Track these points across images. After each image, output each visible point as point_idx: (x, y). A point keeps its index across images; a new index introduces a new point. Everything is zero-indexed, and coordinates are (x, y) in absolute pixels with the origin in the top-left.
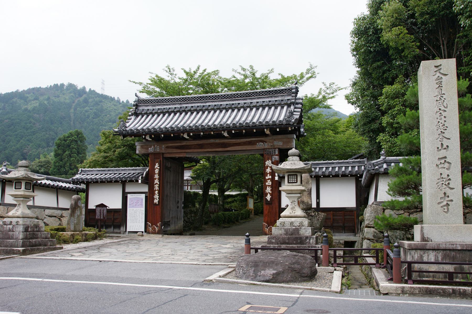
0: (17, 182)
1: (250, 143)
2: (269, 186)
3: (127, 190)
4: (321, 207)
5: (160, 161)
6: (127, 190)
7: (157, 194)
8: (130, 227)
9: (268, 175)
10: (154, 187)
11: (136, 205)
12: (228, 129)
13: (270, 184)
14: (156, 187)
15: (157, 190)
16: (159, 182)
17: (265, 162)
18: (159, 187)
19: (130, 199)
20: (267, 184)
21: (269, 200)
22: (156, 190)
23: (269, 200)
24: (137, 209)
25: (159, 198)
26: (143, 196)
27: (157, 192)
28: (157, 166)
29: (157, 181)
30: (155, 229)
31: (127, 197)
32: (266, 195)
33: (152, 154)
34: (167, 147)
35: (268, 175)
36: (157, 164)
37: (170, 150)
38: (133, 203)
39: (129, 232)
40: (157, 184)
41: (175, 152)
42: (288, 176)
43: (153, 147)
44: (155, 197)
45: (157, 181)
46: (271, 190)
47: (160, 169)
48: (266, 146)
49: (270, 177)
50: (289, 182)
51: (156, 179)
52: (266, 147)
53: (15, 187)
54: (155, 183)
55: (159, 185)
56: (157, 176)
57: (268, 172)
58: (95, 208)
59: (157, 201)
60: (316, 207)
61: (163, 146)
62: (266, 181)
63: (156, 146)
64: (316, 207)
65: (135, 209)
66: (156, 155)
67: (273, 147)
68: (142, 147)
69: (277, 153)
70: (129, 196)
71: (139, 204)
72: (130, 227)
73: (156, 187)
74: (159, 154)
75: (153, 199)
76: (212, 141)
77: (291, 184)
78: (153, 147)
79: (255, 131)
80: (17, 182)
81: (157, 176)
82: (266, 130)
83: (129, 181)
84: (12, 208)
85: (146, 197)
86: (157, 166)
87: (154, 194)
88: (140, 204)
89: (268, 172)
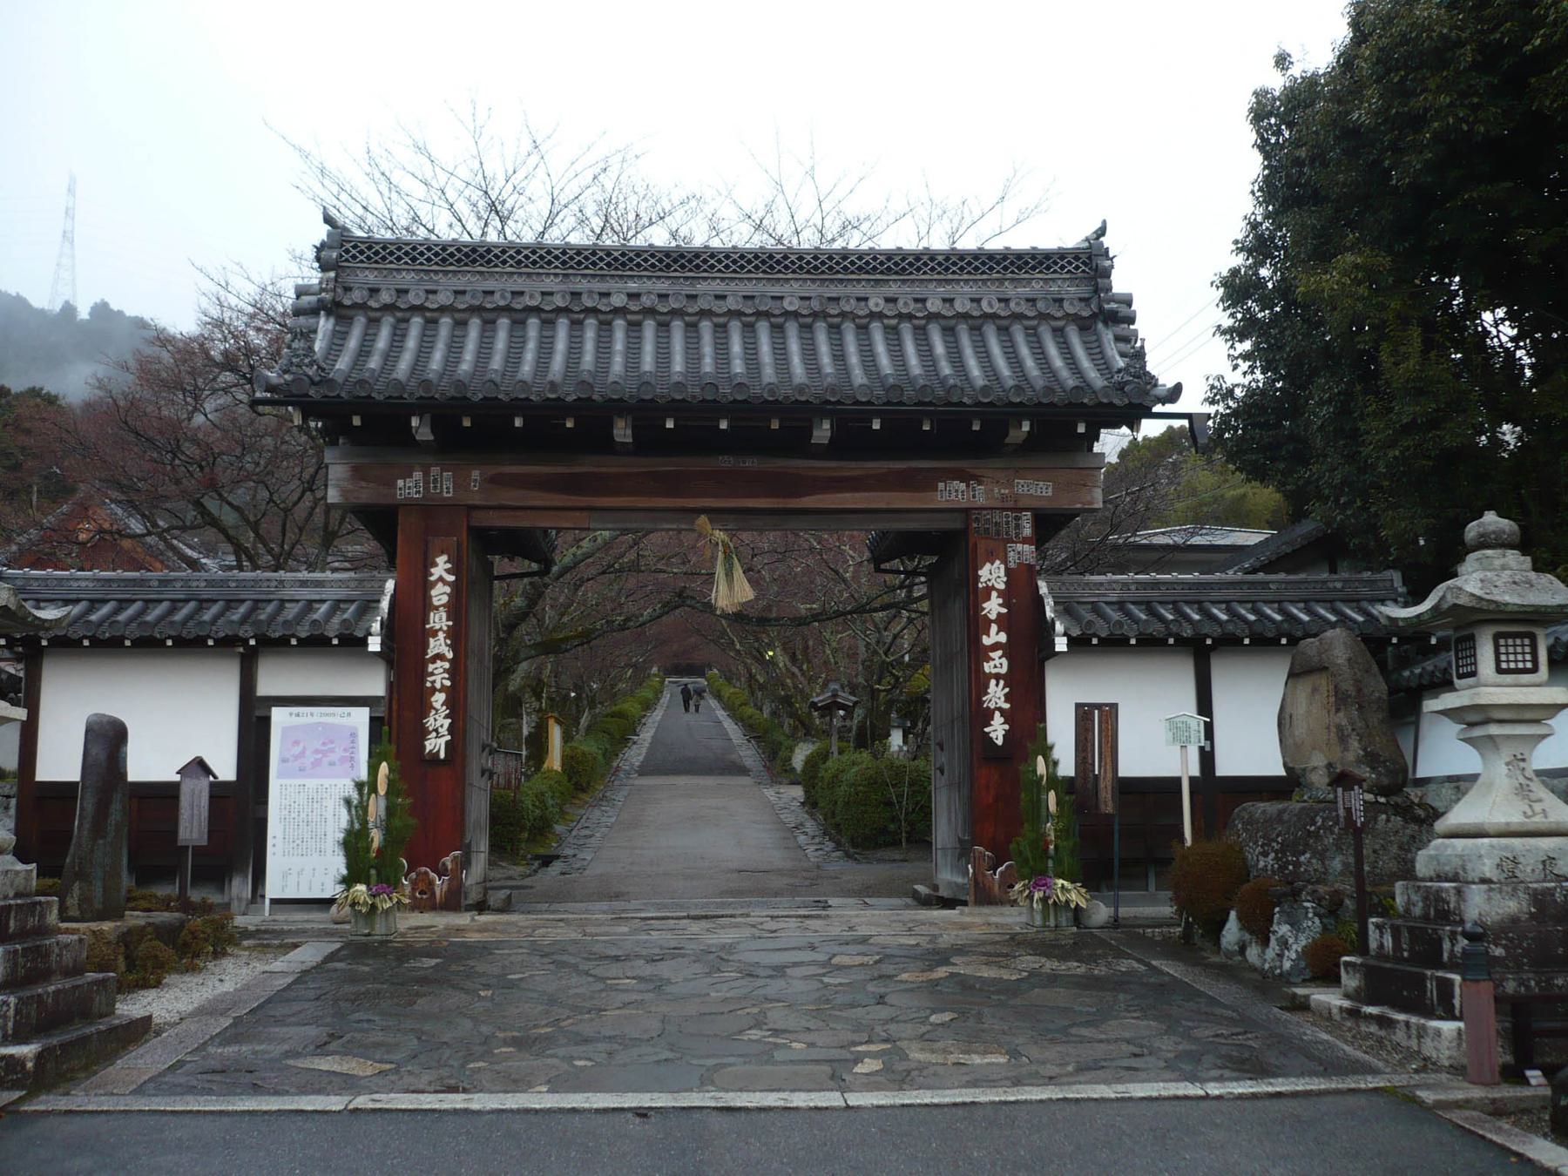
0: (1506, 635)
1: (906, 482)
2: (997, 677)
3: (265, 688)
4: (1219, 773)
5: (459, 545)
6: (265, 688)
7: (444, 711)
8: (285, 875)
9: (994, 628)
10: (423, 674)
11: (317, 763)
12: (645, 411)
13: (1004, 670)
14: (439, 675)
15: (443, 689)
16: (453, 647)
17: (976, 569)
18: (453, 673)
19: (286, 730)
20: (988, 667)
21: (1000, 742)
22: (433, 690)
23: (1000, 742)
24: (327, 782)
25: (451, 730)
26: (361, 716)
27: (439, 699)
28: (441, 568)
29: (439, 645)
30: (431, 883)
31: (266, 721)
32: (987, 716)
33: (410, 505)
34: (495, 481)
35: (994, 628)
36: (442, 560)
37: (510, 497)
38: (303, 753)
39: (274, 901)
40: (439, 657)
41: (557, 503)
42: (1496, 637)
43: (418, 475)
44: (430, 722)
45: (439, 645)
46: (1008, 698)
47: (455, 586)
48: (980, 495)
49: (1003, 638)
50: (1500, 671)
51: (434, 633)
52: (981, 500)
53: (1498, 661)
54: (431, 653)
55: (453, 662)
56: (439, 620)
57: (993, 616)
58: (177, 778)
59: (442, 742)
60: (1072, 773)
61: (476, 474)
62: (982, 654)
63: (435, 470)
64: (1072, 773)
65: (312, 783)
66: (433, 517)
67: (1011, 504)
68: (358, 473)
69: (1027, 531)
70: (278, 715)
71: (333, 757)
72: (285, 875)
73: (439, 675)
74: (449, 507)
75: (423, 733)
76: (726, 462)
77: (1509, 678)
78: (418, 475)
79: (467, 423)
80: (1506, 635)
81: (439, 620)
82: (415, 422)
83: (1104, 642)
84: (1467, 784)
85: (373, 720)
86: (441, 568)
87: (425, 708)
88: (343, 760)
89: (993, 616)
